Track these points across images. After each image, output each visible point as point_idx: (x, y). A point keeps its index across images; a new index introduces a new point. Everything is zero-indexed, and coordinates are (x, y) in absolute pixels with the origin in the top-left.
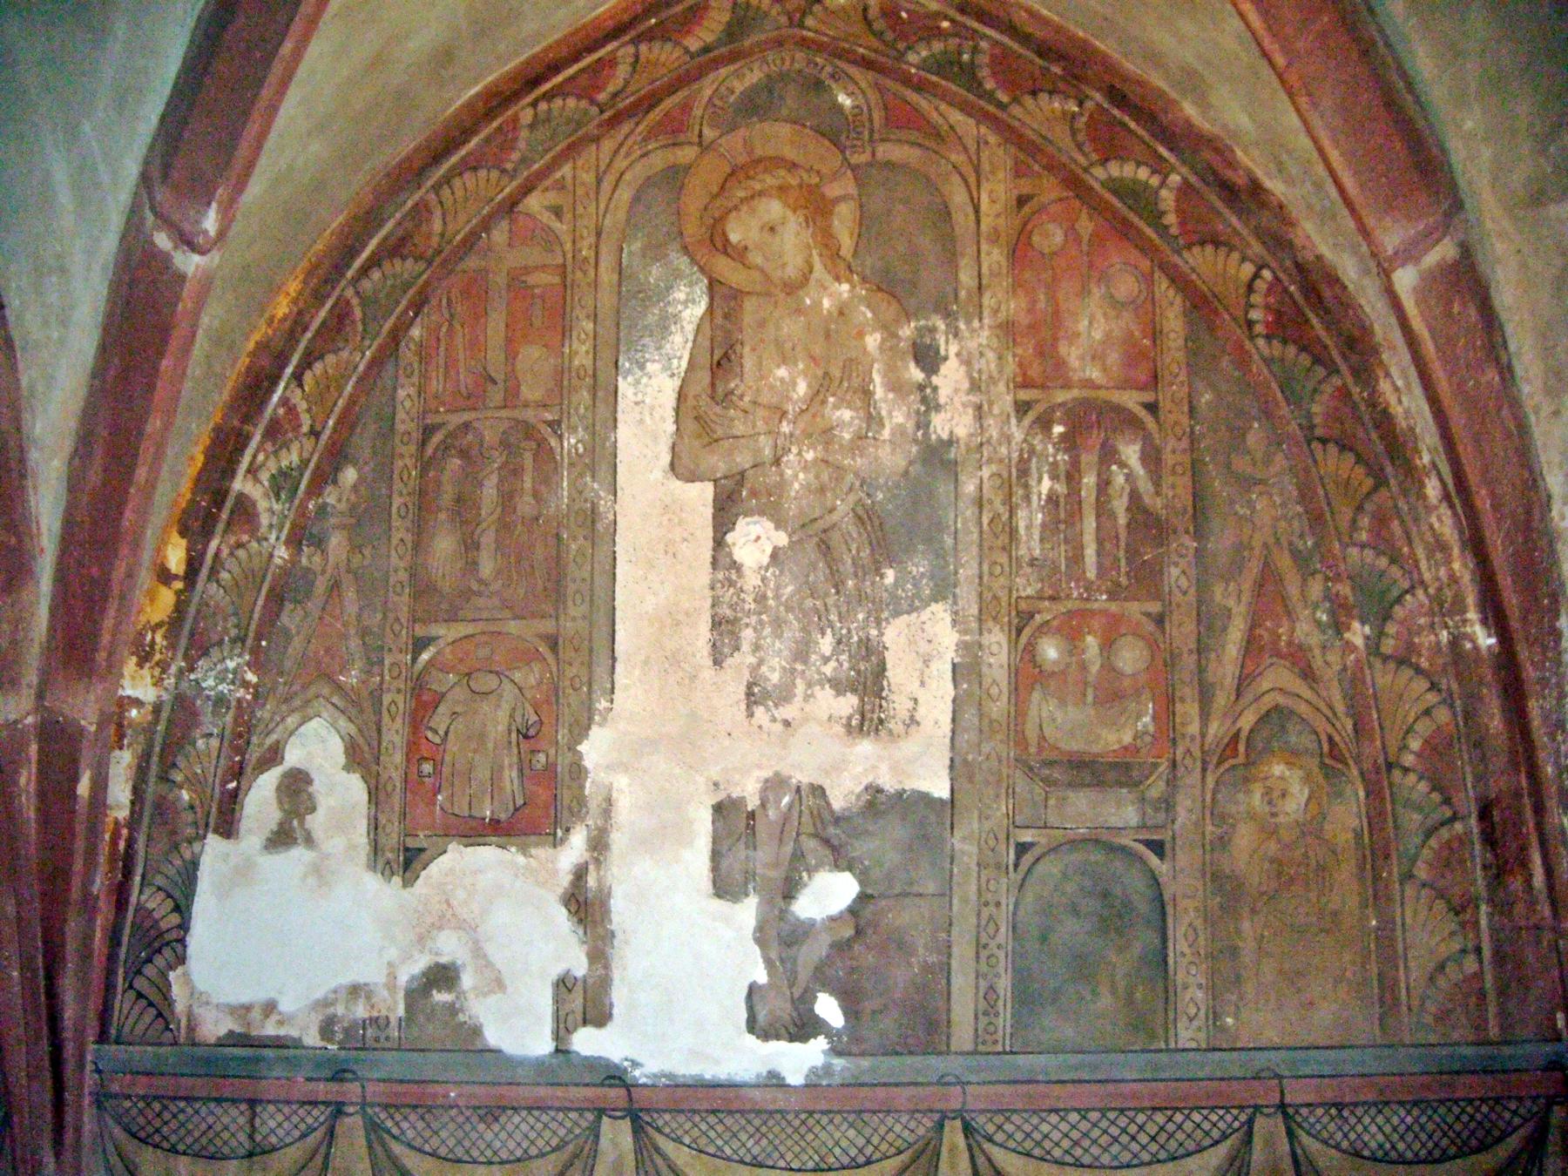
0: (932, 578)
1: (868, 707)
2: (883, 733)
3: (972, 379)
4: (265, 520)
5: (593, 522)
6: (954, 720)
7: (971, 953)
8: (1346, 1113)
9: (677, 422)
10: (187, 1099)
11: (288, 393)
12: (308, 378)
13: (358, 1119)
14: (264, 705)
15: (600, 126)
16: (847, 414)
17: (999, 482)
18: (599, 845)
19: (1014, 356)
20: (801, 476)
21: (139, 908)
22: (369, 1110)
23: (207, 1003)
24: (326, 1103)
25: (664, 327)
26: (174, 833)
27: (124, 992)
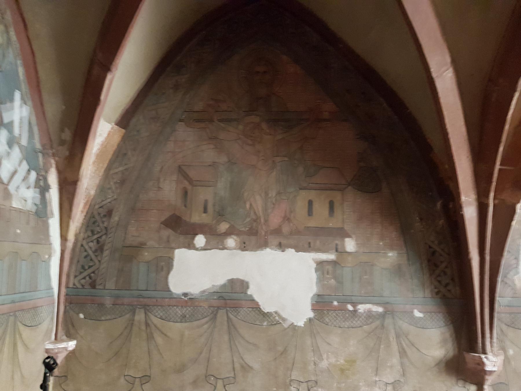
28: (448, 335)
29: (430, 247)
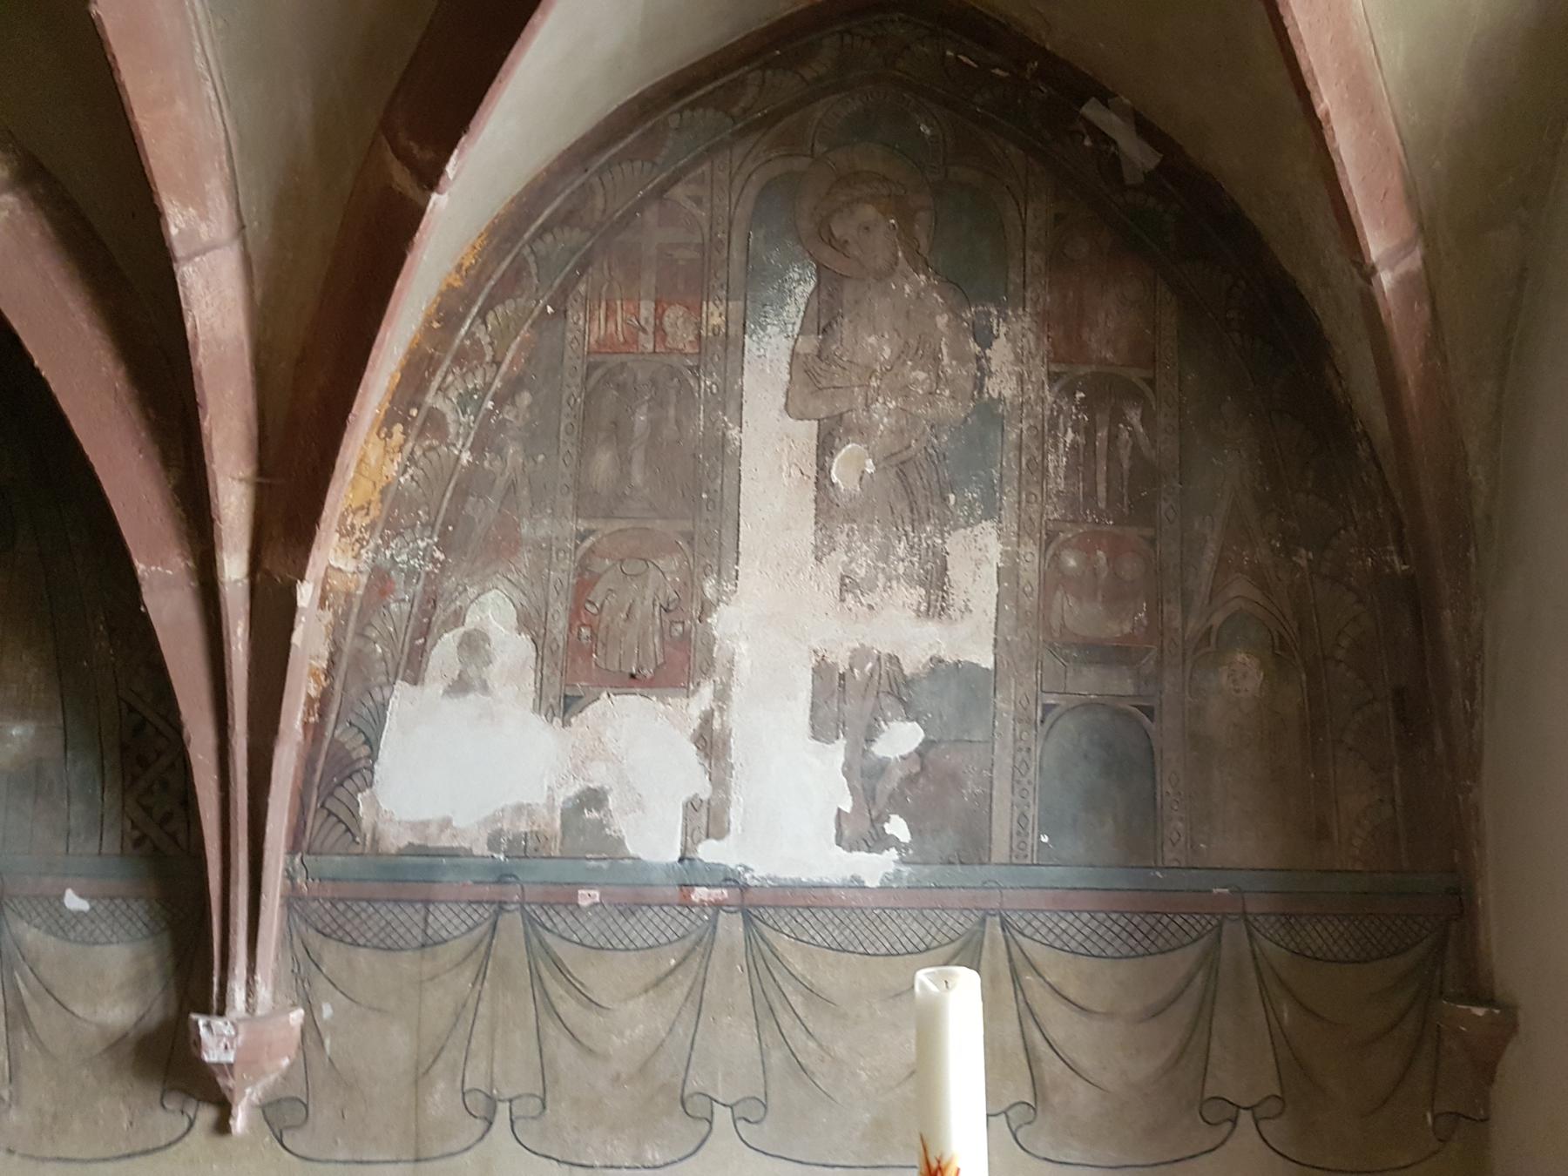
0: (983, 502)
1: (933, 597)
2: (944, 618)
3: (1016, 354)
4: (452, 429)
5: (723, 446)
6: (997, 610)
7: (1008, 787)
8: (1292, 921)
9: (790, 373)
10: (369, 901)
11: (473, 329)
12: (490, 317)
13: (518, 914)
14: (450, 577)
15: (732, 134)
16: (922, 375)
17: (1035, 432)
18: (722, 695)
19: (1048, 337)
20: (885, 420)
21: (333, 740)
22: (527, 908)
23: (391, 820)
24: (491, 902)
25: (783, 295)
26: (367, 679)
27: (316, 811)
28: (151, 962)
29: (132, 709)
